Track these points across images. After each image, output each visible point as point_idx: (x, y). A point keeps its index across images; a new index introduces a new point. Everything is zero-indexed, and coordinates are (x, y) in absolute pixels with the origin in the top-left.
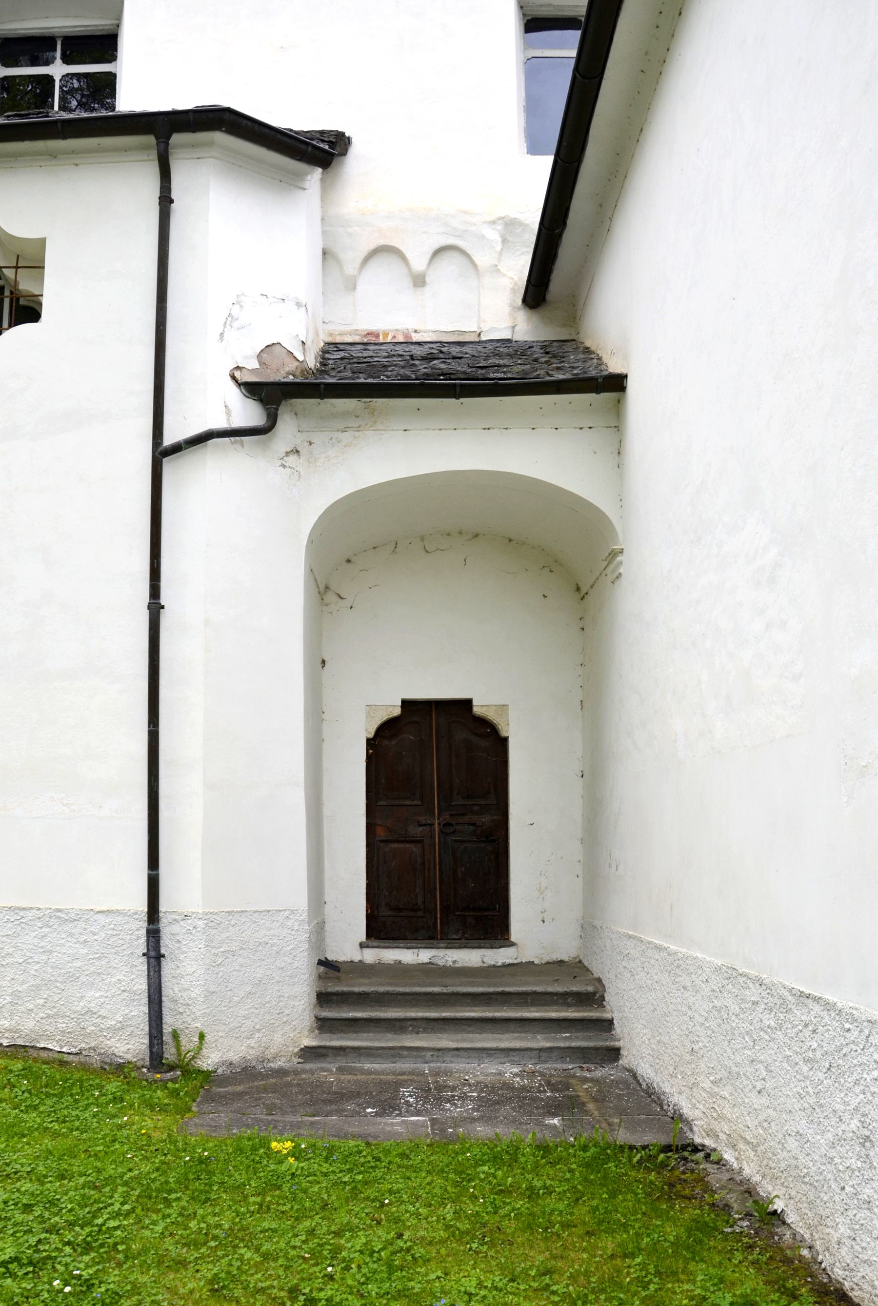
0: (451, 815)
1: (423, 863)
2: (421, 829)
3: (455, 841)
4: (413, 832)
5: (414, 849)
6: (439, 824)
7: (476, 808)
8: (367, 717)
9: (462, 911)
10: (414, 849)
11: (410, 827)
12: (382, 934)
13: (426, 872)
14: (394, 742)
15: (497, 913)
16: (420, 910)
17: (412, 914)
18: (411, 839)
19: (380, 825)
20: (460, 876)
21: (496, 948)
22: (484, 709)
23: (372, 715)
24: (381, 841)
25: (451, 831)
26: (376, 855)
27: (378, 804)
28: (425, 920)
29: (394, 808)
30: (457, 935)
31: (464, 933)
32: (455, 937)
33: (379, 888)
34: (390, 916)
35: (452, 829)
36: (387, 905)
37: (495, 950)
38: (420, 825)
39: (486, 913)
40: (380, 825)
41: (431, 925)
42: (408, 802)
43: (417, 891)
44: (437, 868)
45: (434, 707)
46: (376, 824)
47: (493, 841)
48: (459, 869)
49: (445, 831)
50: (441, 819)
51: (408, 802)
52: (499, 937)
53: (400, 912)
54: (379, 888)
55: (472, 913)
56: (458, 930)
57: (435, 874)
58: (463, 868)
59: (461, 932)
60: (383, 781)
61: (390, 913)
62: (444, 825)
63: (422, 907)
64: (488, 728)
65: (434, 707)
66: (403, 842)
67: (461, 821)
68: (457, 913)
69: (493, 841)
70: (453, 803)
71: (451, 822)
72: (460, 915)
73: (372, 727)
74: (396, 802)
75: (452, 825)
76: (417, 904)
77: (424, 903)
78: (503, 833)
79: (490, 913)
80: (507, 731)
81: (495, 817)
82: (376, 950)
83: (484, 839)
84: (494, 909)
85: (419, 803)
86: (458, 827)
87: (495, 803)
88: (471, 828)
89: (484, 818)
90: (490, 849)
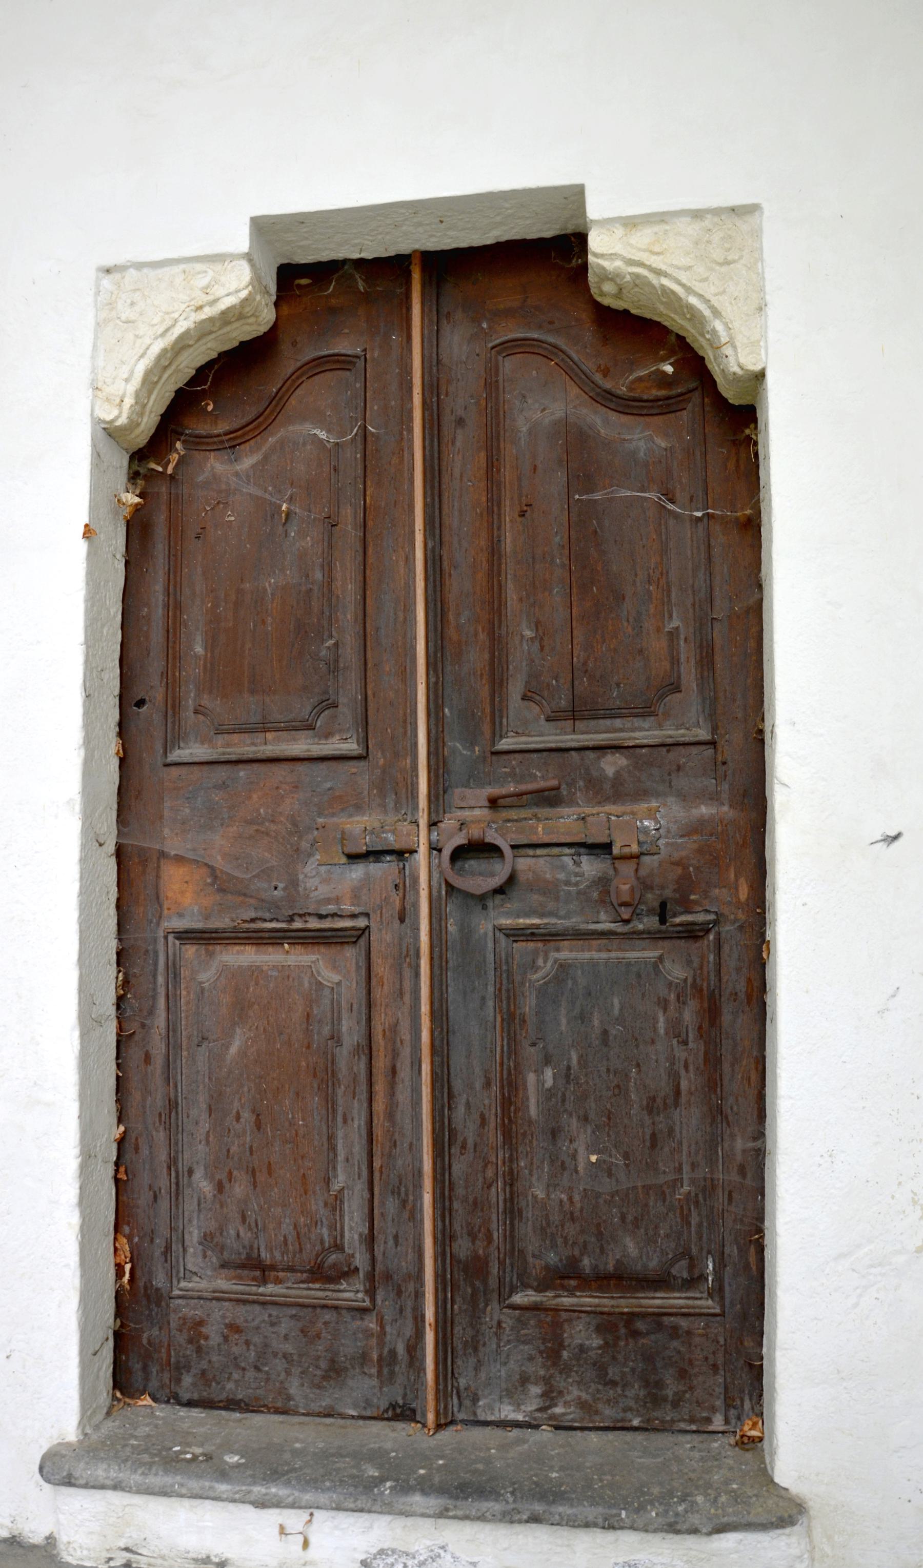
0: (493, 803)
1: (368, 1048)
2: (358, 872)
3: (516, 934)
4: (323, 891)
5: (329, 976)
6: (435, 848)
7: (611, 765)
8: (99, 326)
9: (541, 1288)
10: (329, 976)
11: (311, 867)
12: (187, 1380)
13: (380, 1087)
14: (248, 462)
15: (709, 1305)
16: (350, 1272)
17: (316, 1293)
18: (313, 924)
19: (180, 859)
20: (533, 1111)
21: (694, 1531)
22: (643, 238)
23: (127, 313)
24: (185, 936)
25: (496, 881)
26: (161, 1002)
27: (176, 755)
28: (372, 1324)
29: (242, 773)
30: (518, 1407)
31: (550, 1396)
32: (508, 1412)
33: (172, 1163)
34: (219, 1297)
35: (499, 873)
36: (207, 1239)
37: (691, 1542)
38: (353, 858)
39: (656, 1301)
40: (180, 859)
41: (401, 1349)
42: (300, 746)
43: (340, 1180)
44: (426, 1068)
45: (416, 276)
46: (162, 855)
47: (692, 933)
48: (531, 1078)
49: (457, 882)
50: (449, 823)
51: (300, 746)
52: (718, 1423)
53: (264, 1281)
54: (172, 1163)
55: (587, 1300)
56: (524, 1380)
57: (416, 1103)
58: (549, 1073)
59: (535, 1390)
60: (199, 649)
61: (223, 1284)
62: (459, 854)
63: (360, 1260)
64: (663, 360)
65: (416, 276)
66: (275, 939)
67: (541, 833)
68: (518, 1298)
69: (692, 933)
70: (504, 744)
71: (492, 837)
72: (535, 1308)
73: (124, 372)
74: (246, 747)
75: (492, 850)
76: (338, 1247)
77: (370, 1240)
78: (744, 893)
79: (676, 1300)
80: (755, 344)
81: (704, 810)
82: (116, 1499)
83: (650, 922)
84: (694, 1281)
85: (351, 746)
86: (523, 864)
87: (703, 734)
88: (590, 867)
89: (651, 814)
90: (676, 972)
